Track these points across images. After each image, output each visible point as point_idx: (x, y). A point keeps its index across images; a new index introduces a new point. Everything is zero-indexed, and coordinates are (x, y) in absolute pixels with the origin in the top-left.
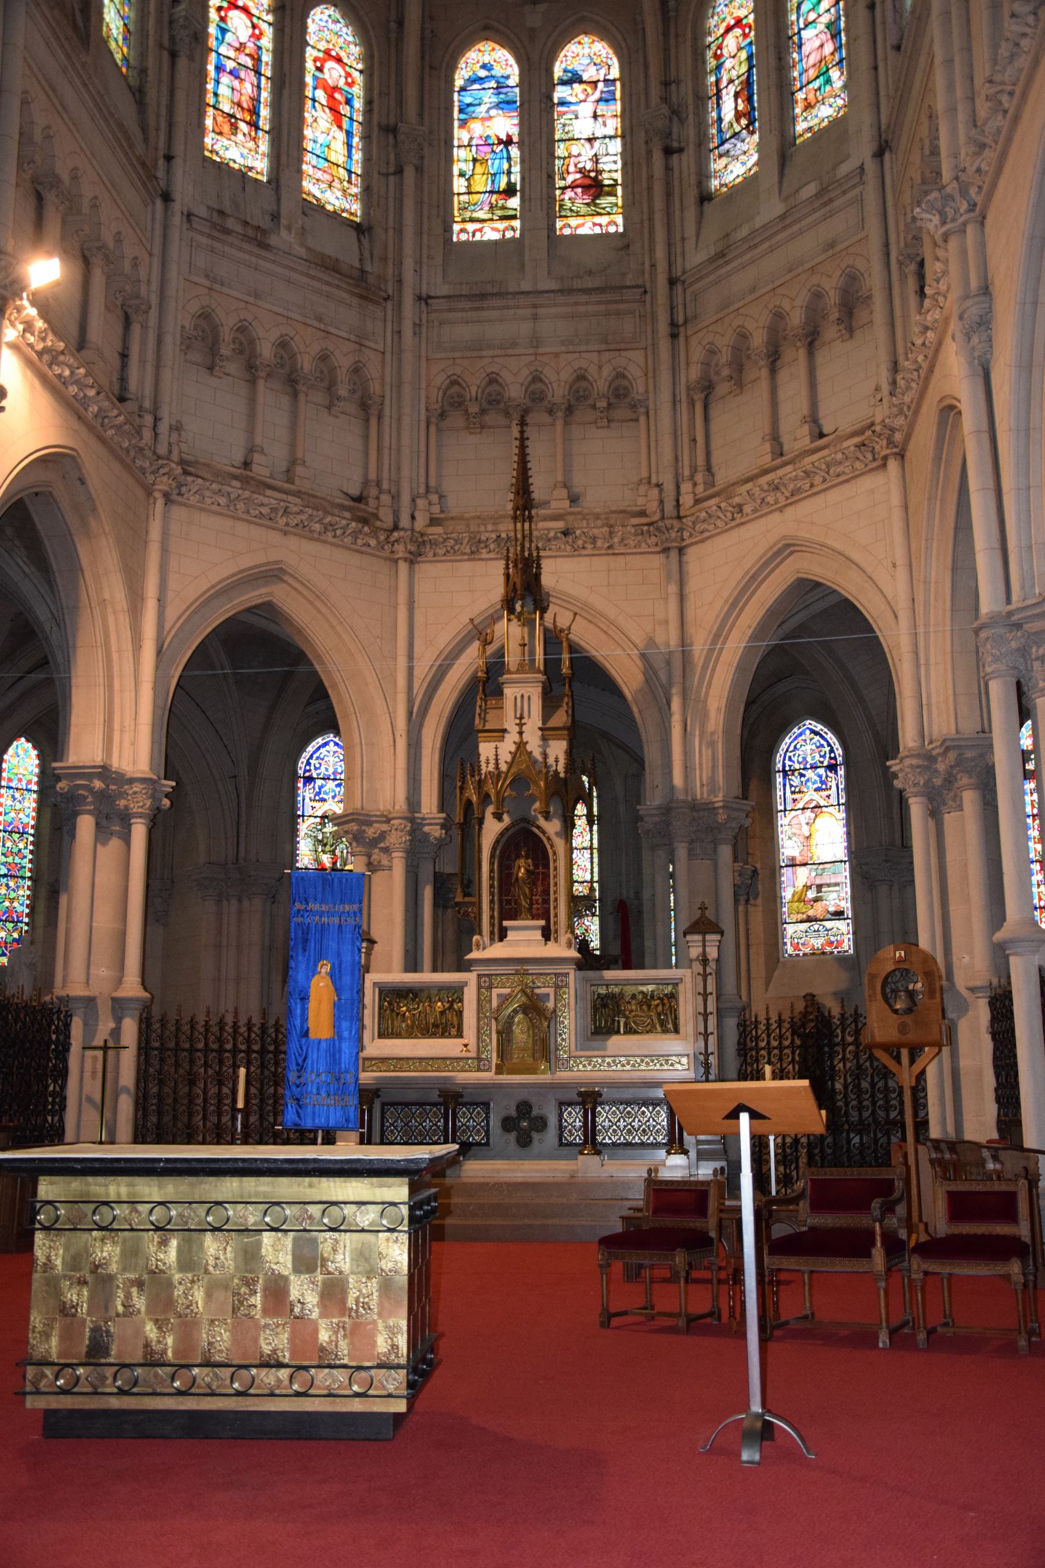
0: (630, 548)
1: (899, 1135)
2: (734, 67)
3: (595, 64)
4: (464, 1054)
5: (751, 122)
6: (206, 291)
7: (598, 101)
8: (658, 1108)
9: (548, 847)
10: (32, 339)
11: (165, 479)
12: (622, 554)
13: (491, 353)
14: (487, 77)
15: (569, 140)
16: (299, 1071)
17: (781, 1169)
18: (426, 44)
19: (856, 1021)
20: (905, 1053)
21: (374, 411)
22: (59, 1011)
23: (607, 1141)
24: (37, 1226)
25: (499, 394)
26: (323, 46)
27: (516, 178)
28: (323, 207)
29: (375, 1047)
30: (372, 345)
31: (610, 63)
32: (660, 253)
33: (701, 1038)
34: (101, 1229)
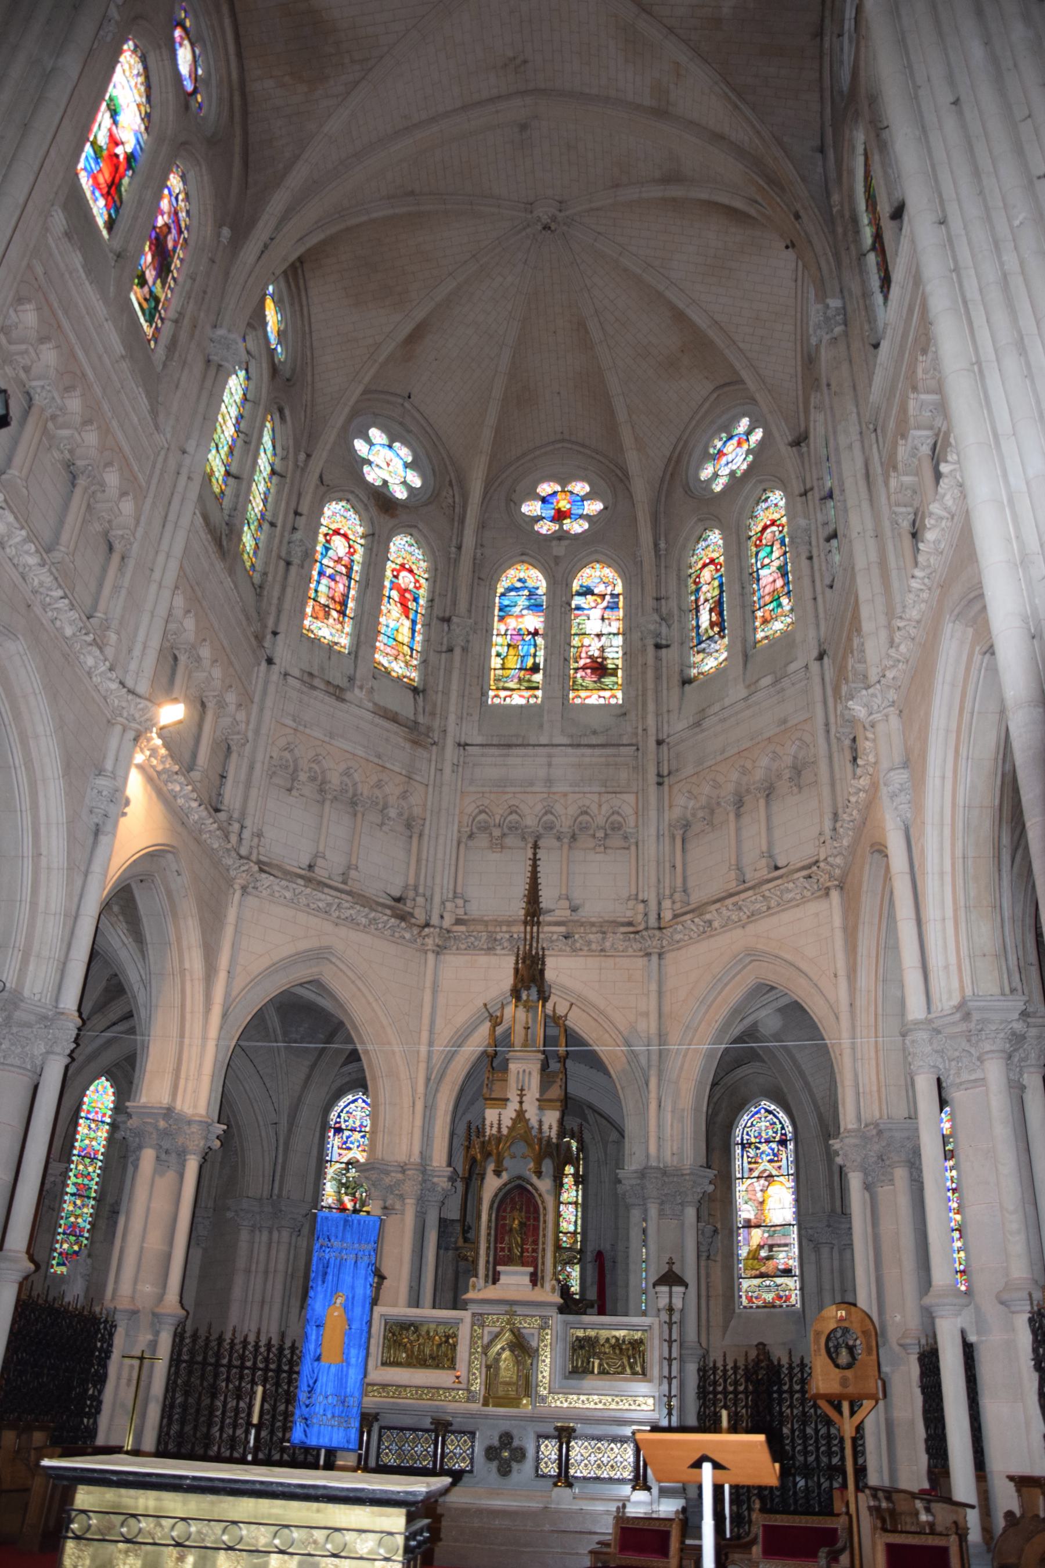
1: (840, 1480)
2: (709, 591)
4: (457, 1386)
5: (722, 629)
6: (292, 731)
7: (605, 608)
8: (625, 1445)
9: (539, 1202)
10: (154, 762)
11: (244, 875)
13: (513, 789)
16: (309, 1392)
17: (735, 1508)
18: (477, 566)
19: (802, 1371)
20: (846, 1407)
21: (416, 830)
22: (106, 1321)
23: (578, 1474)
24: (70, 1535)
26: (399, 561)
27: (540, 660)
28: (389, 673)
29: (379, 1374)
30: (418, 778)
32: (651, 721)
33: (665, 1381)
34: (128, 1541)
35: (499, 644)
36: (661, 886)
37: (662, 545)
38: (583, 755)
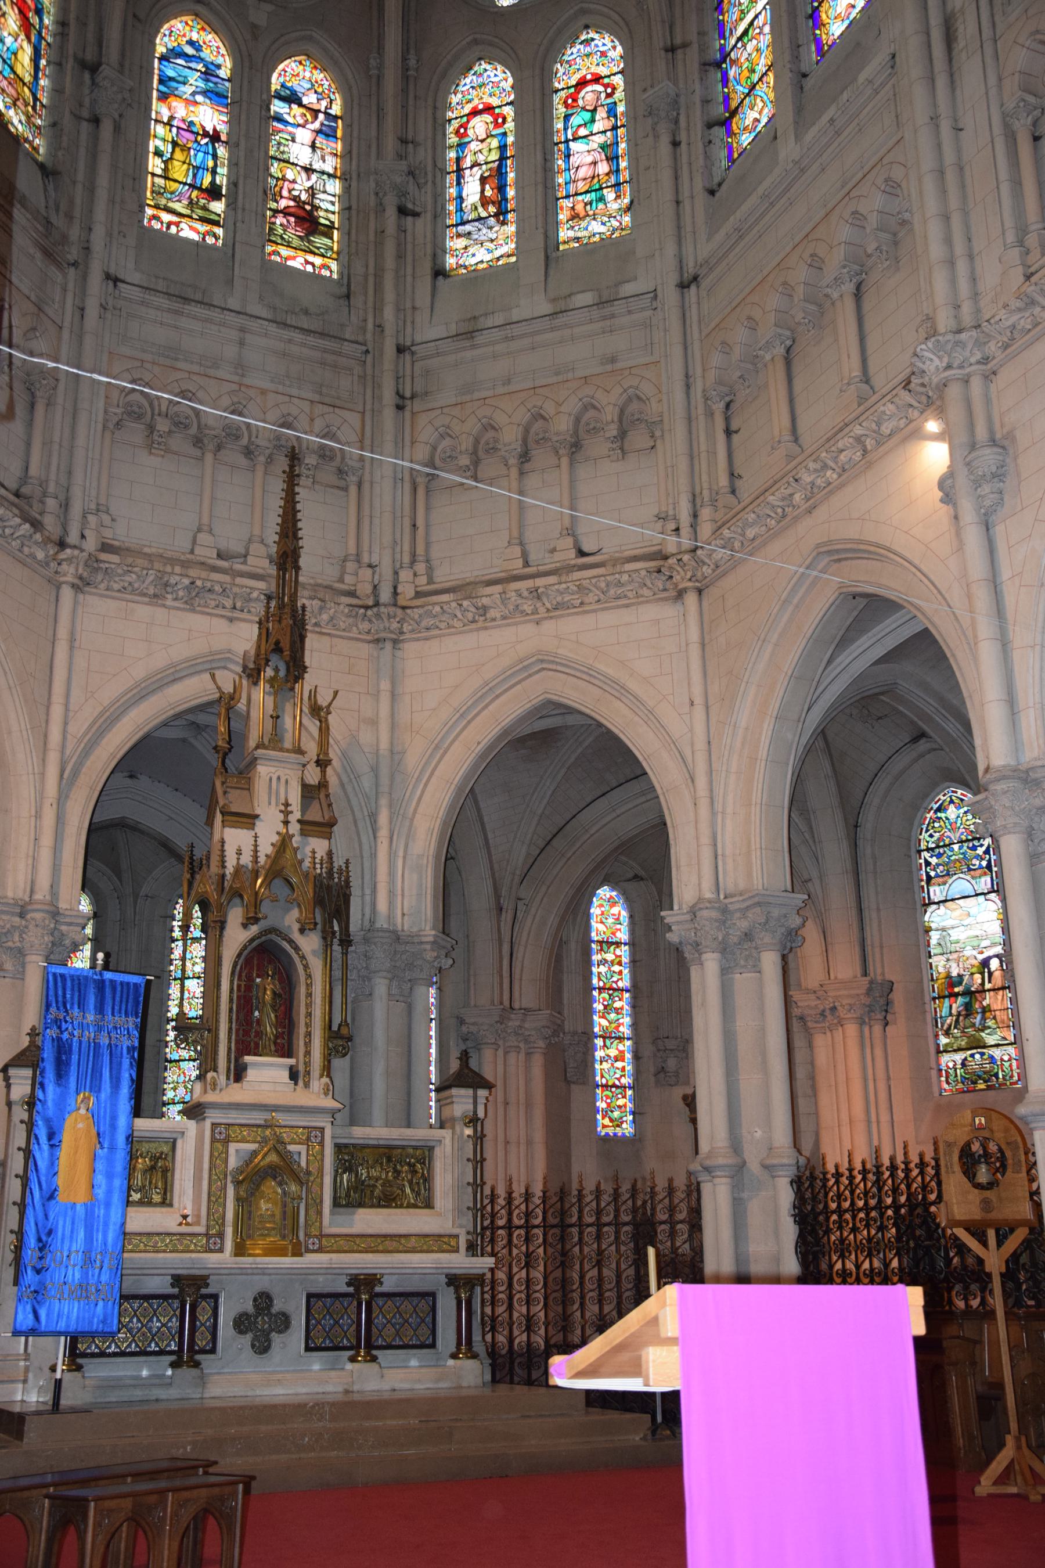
0: (337, 630)
3: (316, 92)
7: (318, 132)
12: (329, 634)
14: (193, 56)
15: (284, 161)
25: (187, 418)
27: (222, 180)
31: (333, 97)
35: (160, 137)
36: (398, 549)
37: (412, 63)
38: (290, 341)
